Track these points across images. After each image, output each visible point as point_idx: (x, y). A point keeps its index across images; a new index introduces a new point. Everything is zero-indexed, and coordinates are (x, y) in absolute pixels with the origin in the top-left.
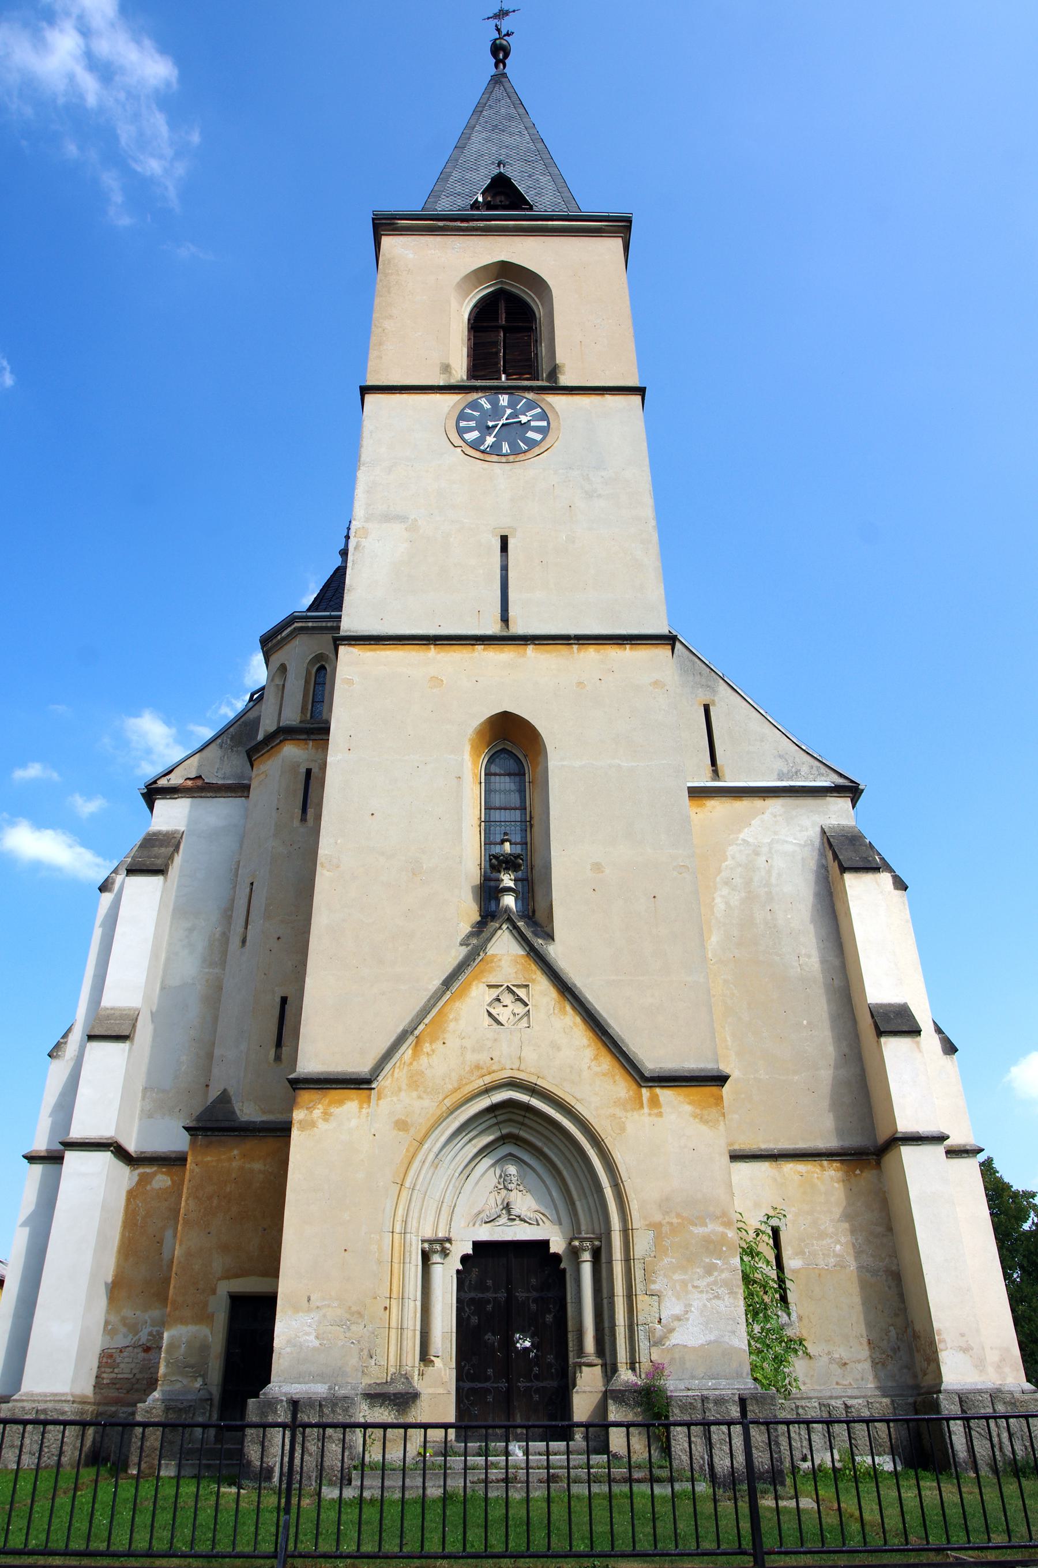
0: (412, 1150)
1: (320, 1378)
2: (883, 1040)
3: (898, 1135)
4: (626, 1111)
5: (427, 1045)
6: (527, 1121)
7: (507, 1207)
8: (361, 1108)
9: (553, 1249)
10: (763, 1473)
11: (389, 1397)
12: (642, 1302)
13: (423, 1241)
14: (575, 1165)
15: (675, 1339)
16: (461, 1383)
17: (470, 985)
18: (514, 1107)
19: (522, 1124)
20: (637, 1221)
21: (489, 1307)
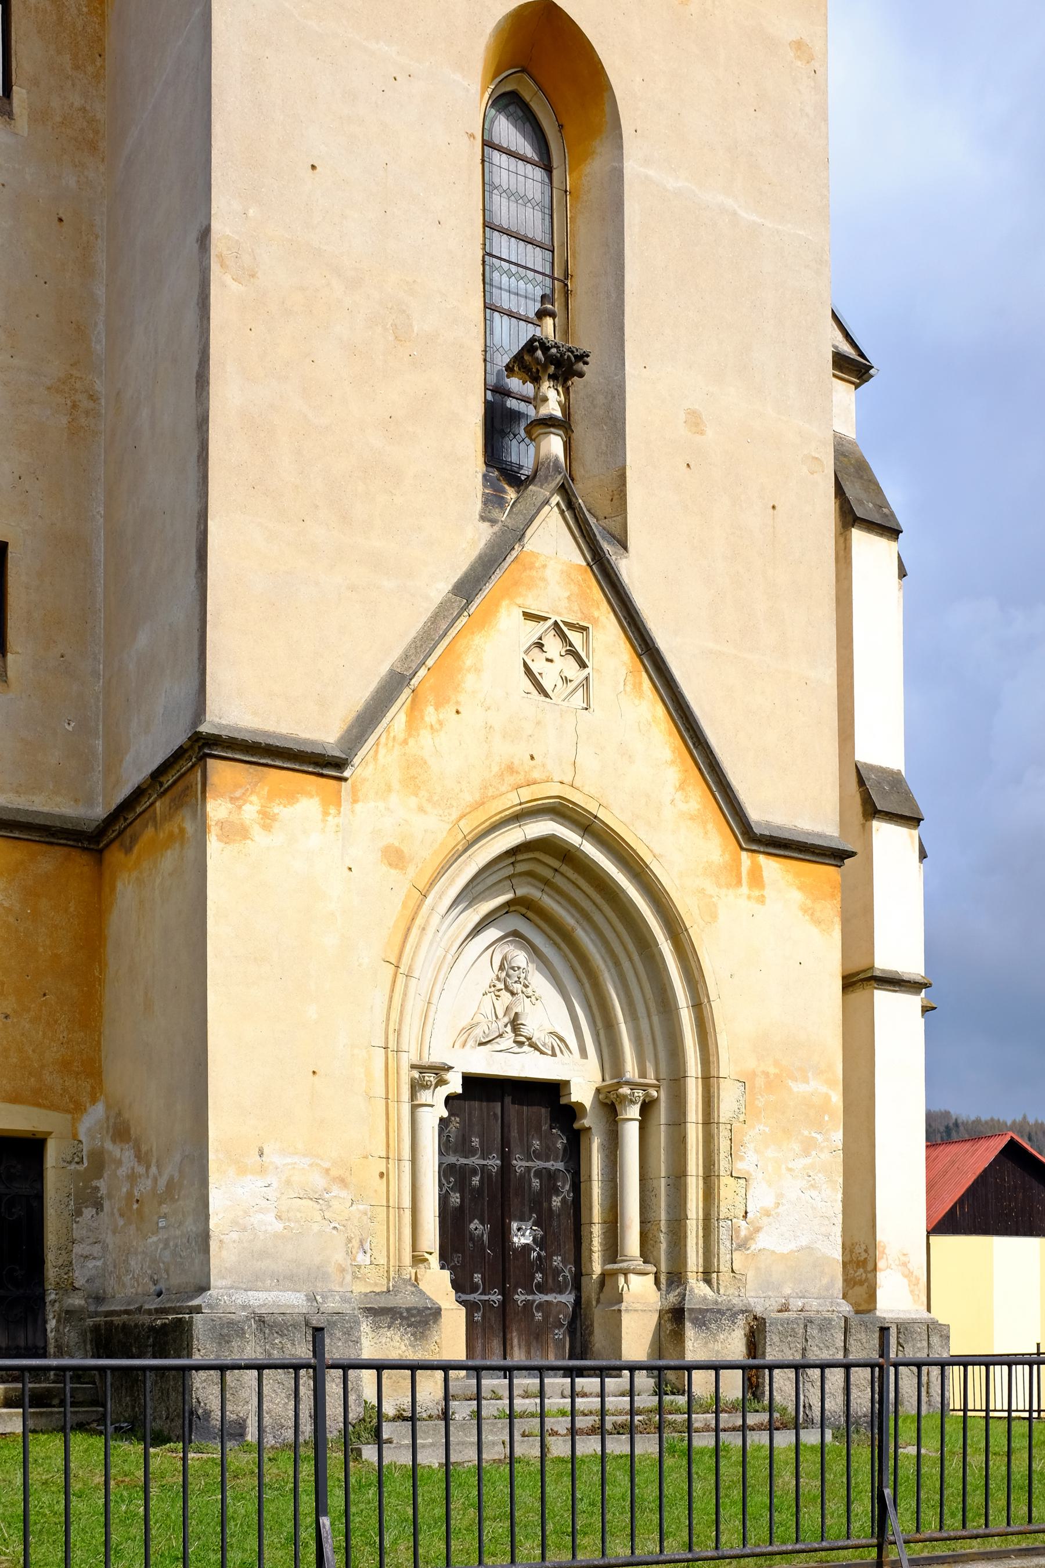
0: (412, 904)
1: (288, 1280)
2: (876, 824)
3: (877, 973)
4: (719, 886)
5: (430, 709)
6: (559, 880)
7: (515, 1024)
8: (326, 813)
10: (860, 1417)
11: (401, 1314)
12: (727, 1189)
13: (413, 1067)
14: (626, 965)
15: (761, 1241)
17: (497, 605)
19: (547, 882)
20: (726, 1066)
21: (476, 1181)
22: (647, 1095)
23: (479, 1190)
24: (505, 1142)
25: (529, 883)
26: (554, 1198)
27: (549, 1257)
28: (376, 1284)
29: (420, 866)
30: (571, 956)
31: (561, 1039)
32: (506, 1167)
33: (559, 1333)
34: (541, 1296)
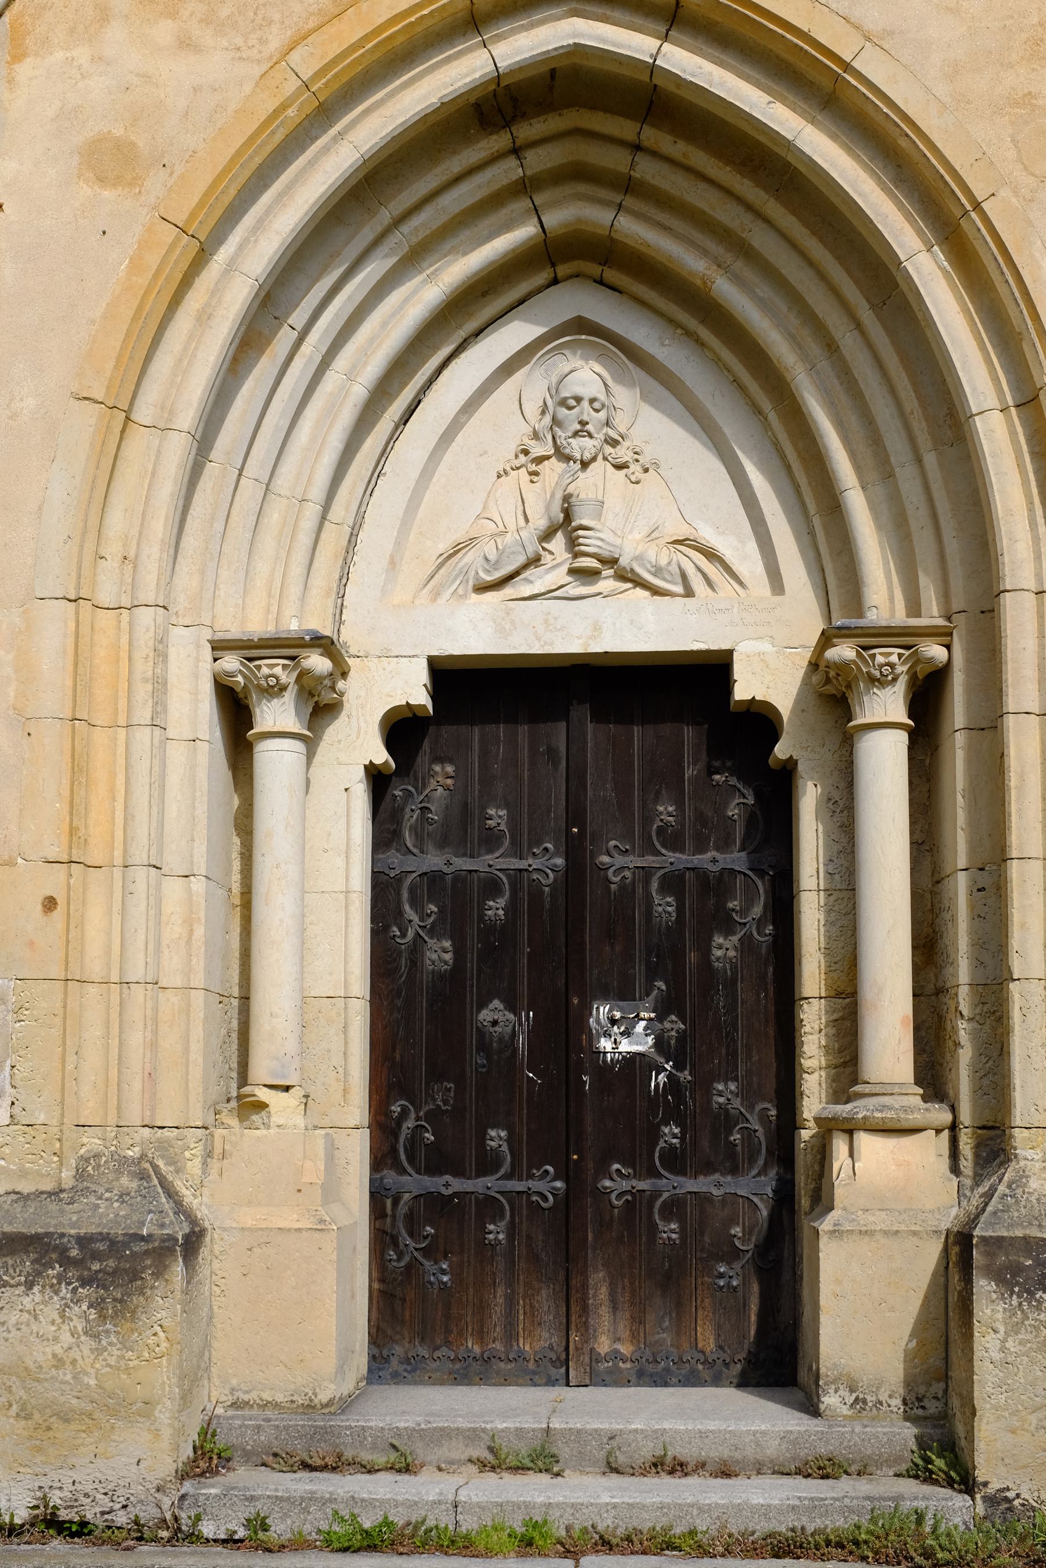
6: (647, 170)
7: (566, 523)
9: (745, 688)
11: (63, 1251)
13: (220, 647)
14: (848, 341)
16: (390, 1177)
18: (594, 106)
21: (496, 908)
22: (917, 659)
23: (506, 931)
24: (575, 813)
25: (579, 197)
26: (719, 940)
27: (703, 1084)
28: (23, 1174)
29: (179, 170)
30: (727, 356)
31: (711, 555)
32: (579, 870)
33: (730, 1274)
34: (677, 1180)
